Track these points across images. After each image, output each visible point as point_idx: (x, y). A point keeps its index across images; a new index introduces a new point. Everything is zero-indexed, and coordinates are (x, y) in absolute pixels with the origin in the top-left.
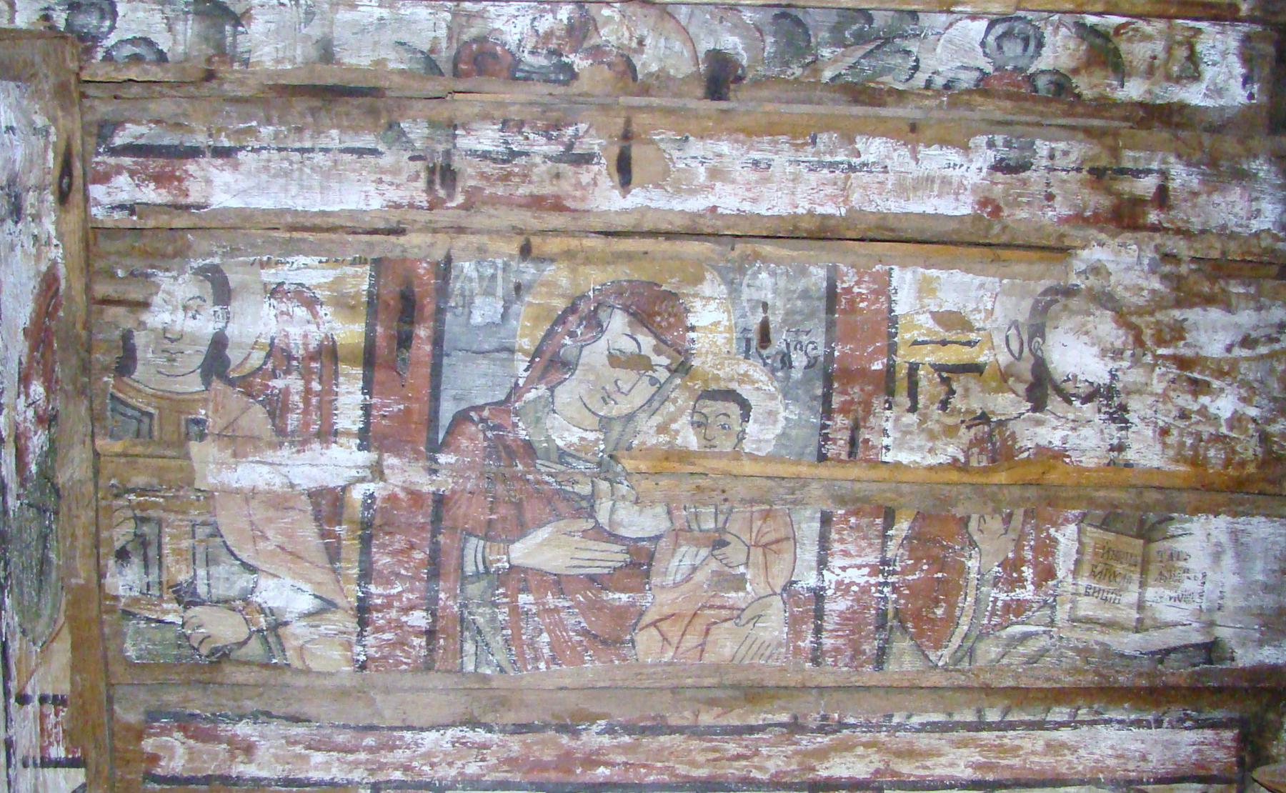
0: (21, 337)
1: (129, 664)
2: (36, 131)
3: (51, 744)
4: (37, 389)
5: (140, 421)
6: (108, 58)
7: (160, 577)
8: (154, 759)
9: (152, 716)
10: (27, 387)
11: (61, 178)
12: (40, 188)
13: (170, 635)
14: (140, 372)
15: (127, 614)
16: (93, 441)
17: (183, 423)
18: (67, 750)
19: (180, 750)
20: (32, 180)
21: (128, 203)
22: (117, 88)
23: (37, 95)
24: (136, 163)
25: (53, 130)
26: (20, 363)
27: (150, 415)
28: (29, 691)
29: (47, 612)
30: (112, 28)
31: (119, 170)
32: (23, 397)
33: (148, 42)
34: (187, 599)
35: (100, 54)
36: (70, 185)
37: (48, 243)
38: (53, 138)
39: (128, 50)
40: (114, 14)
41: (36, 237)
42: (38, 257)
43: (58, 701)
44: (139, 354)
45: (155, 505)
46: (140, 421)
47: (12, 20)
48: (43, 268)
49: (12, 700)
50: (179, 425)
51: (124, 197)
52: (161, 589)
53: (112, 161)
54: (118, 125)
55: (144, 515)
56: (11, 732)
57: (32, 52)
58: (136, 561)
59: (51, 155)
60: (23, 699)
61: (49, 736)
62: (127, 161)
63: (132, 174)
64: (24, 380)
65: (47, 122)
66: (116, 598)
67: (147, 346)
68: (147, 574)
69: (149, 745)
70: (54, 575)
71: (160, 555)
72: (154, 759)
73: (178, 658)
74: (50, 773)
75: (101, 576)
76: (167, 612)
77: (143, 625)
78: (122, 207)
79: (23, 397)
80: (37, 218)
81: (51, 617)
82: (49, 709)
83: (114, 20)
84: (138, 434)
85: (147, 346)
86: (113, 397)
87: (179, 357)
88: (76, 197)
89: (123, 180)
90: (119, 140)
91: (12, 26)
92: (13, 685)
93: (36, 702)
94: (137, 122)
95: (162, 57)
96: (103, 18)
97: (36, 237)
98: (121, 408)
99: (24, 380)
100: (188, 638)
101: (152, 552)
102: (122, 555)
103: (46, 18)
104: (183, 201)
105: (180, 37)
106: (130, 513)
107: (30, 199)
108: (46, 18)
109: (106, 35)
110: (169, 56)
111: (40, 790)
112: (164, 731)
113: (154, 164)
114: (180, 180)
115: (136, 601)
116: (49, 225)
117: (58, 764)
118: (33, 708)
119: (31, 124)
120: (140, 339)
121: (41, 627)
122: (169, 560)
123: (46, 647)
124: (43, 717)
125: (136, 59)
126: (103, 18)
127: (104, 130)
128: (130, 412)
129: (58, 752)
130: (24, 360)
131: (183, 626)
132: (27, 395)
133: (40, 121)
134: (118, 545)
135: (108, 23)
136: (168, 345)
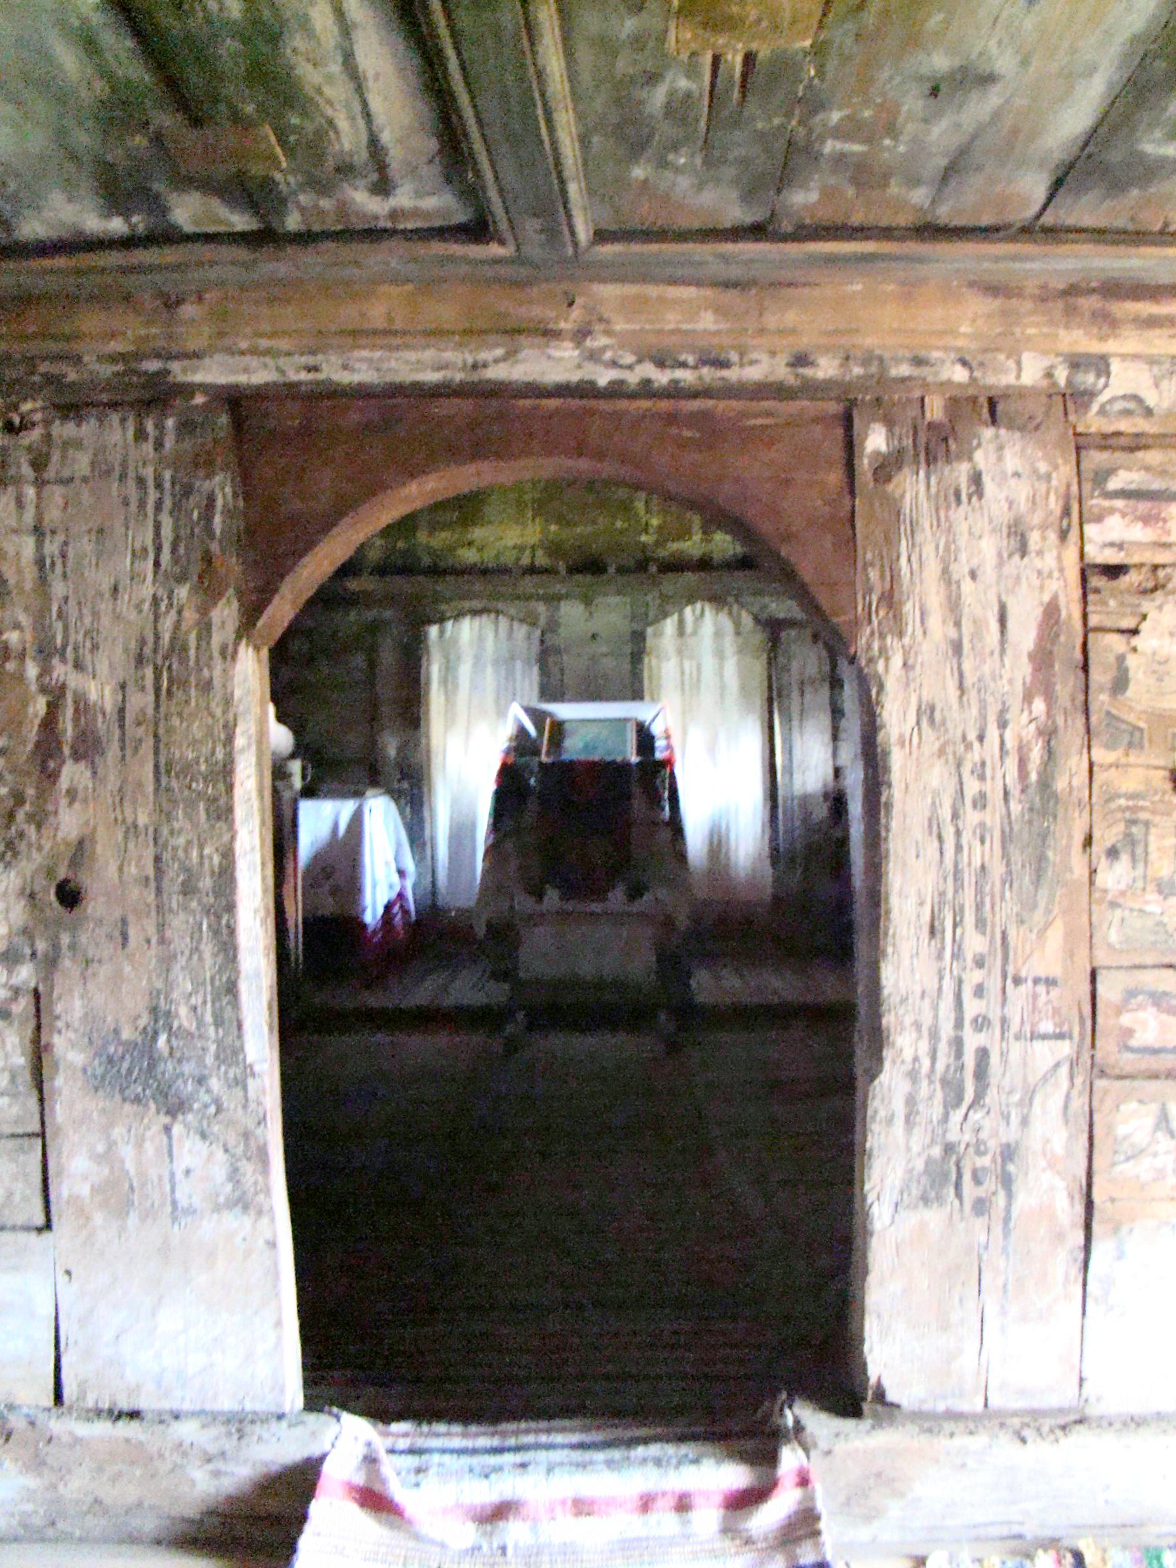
0: (1025, 660)
1: (1110, 946)
2: (1039, 478)
3: (1041, 1019)
4: (1039, 706)
5: (1132, 735)
6: (1102, 411)
7: (1145, 872)
8: (1129, 1032)
9: (1131, 994)
10: (1030, 703)
11: (1062, 518)
12: (1044, 527)
13: (1150, 923)
14: (1130, 693)
15: (1114, 905)
16: (1089, 752)
17: (1170, 737)
18: (1056, 1025)
19: (1153, 1024)
20: (1037, 519)
21: (1118, 542)
22: (1107, 441)
23: (1043, 445)
24: (1126, 506)
25: (1054, 475)
26: (1024, 683)
27: (1141, 730)
28: (1023, 974)
29: (1042, 904)
30: (1106, 386)
31: (1112, 511)
32: (1026, 713)
33: (1136, 398)
34: (1166, 891)
35: (1095, 408)
36: (1069, 525)
37: (1050, 576)
38: (1054, 483)
39: (1119, 406)
40: (1108, 375)
41: (1039, 573)
42: (1042, 588)
43: (1051, 982)
44: (1131, 674)
45: (1142, 808)
46: (1132, 735)
47: (1018, 377)
48: (1046, 598)
49: (1009, 981)
50: (1166, 737)
51: (1115, 536)
52: (1145, 883)
53: (1106, 503)
54: (1111, 472)
55: (1134, 817)
56: (1006, 1010)
57: (1035, 407)
58: (1125, 858)
59: (1052, 498)
60: (1017, 981)
61: (1040, 1012)
62: (1119, 503)
63: (1124, 515)
64: (1028, 698)
65: (1050, 469)
66: (1105, 891)
67: (1138, 667)
68: (1134, 868)
69: (1126, 1020)
70: (1050, 870)
71: (1147, 853)
72: (1129, 1032)
73: (1154, 943)
74: (1038, 1045)
75: (1093, 872)
76: (1147, 902)
77: (1127, 913)
78: (1112, 545)
79: (1026, 713)
80: (1040, 553)
81: (1046, 908)
82: (1041, 989)
83: (1108, 377)
84: (1130, 745)
85: (1138, 667)
86: (1108, 713)
87: (1166, 678)
88: (1074, 535)
89: (1114, 521)
90: (1113, 484)
91: (1018, 383)
92: (1011, 970)
93: (1030, 983)
94: (1129, 469)
95: (1149, 412)
96: (1098, 376)
97: (1039, 573)
98: (1114, 723)
99: (1028, 698)
100: (1165, 925)
101: (1139, 850)
102: (1113, 853)
103: (1049, 375)
104: (1164, 539)
105: (1165, 394)
106: (1119, 815)
107: (1034, 538)
108: (1049, 375)
109: (1101, 392)
110: (1155, 411)
111: (1166, 1062)
112: (1140, 1007)
113: (1143, 507)
114: (1165, 521)
115: (1123, 893)
116: (1049, 561)
117: (1044, 1037)
118: (1026, 988)
119: (1035, 471)
120: (1132, 661)
121: (1038, 916)
122: (1153, 856)
123: (1042, 932)
124: (1035, 997)
125: (1127, 413)
126: (1098, 376)
127: (1101, 477)
128: (1123, 726)
129: (1047, 1027)
130: (1028, 680)
131: (1162, 914)
132: (1031, 712)
133: (1043, 467)
134: (1108, 844)
135: (1102, 381)
136: (1157, 667)
